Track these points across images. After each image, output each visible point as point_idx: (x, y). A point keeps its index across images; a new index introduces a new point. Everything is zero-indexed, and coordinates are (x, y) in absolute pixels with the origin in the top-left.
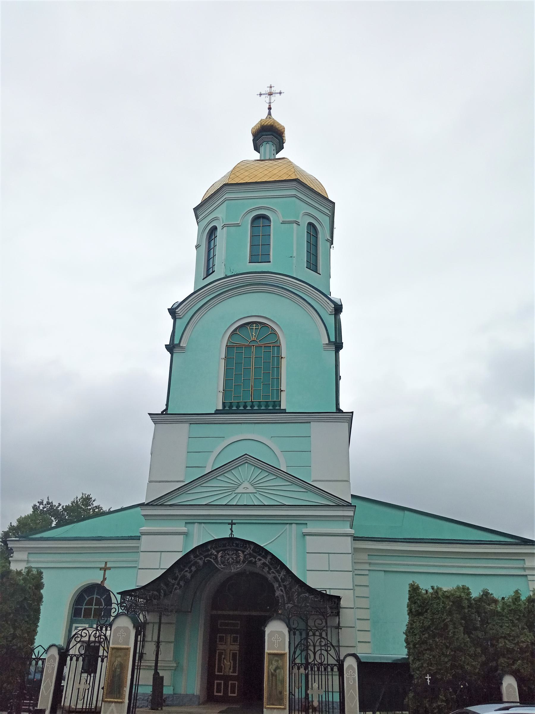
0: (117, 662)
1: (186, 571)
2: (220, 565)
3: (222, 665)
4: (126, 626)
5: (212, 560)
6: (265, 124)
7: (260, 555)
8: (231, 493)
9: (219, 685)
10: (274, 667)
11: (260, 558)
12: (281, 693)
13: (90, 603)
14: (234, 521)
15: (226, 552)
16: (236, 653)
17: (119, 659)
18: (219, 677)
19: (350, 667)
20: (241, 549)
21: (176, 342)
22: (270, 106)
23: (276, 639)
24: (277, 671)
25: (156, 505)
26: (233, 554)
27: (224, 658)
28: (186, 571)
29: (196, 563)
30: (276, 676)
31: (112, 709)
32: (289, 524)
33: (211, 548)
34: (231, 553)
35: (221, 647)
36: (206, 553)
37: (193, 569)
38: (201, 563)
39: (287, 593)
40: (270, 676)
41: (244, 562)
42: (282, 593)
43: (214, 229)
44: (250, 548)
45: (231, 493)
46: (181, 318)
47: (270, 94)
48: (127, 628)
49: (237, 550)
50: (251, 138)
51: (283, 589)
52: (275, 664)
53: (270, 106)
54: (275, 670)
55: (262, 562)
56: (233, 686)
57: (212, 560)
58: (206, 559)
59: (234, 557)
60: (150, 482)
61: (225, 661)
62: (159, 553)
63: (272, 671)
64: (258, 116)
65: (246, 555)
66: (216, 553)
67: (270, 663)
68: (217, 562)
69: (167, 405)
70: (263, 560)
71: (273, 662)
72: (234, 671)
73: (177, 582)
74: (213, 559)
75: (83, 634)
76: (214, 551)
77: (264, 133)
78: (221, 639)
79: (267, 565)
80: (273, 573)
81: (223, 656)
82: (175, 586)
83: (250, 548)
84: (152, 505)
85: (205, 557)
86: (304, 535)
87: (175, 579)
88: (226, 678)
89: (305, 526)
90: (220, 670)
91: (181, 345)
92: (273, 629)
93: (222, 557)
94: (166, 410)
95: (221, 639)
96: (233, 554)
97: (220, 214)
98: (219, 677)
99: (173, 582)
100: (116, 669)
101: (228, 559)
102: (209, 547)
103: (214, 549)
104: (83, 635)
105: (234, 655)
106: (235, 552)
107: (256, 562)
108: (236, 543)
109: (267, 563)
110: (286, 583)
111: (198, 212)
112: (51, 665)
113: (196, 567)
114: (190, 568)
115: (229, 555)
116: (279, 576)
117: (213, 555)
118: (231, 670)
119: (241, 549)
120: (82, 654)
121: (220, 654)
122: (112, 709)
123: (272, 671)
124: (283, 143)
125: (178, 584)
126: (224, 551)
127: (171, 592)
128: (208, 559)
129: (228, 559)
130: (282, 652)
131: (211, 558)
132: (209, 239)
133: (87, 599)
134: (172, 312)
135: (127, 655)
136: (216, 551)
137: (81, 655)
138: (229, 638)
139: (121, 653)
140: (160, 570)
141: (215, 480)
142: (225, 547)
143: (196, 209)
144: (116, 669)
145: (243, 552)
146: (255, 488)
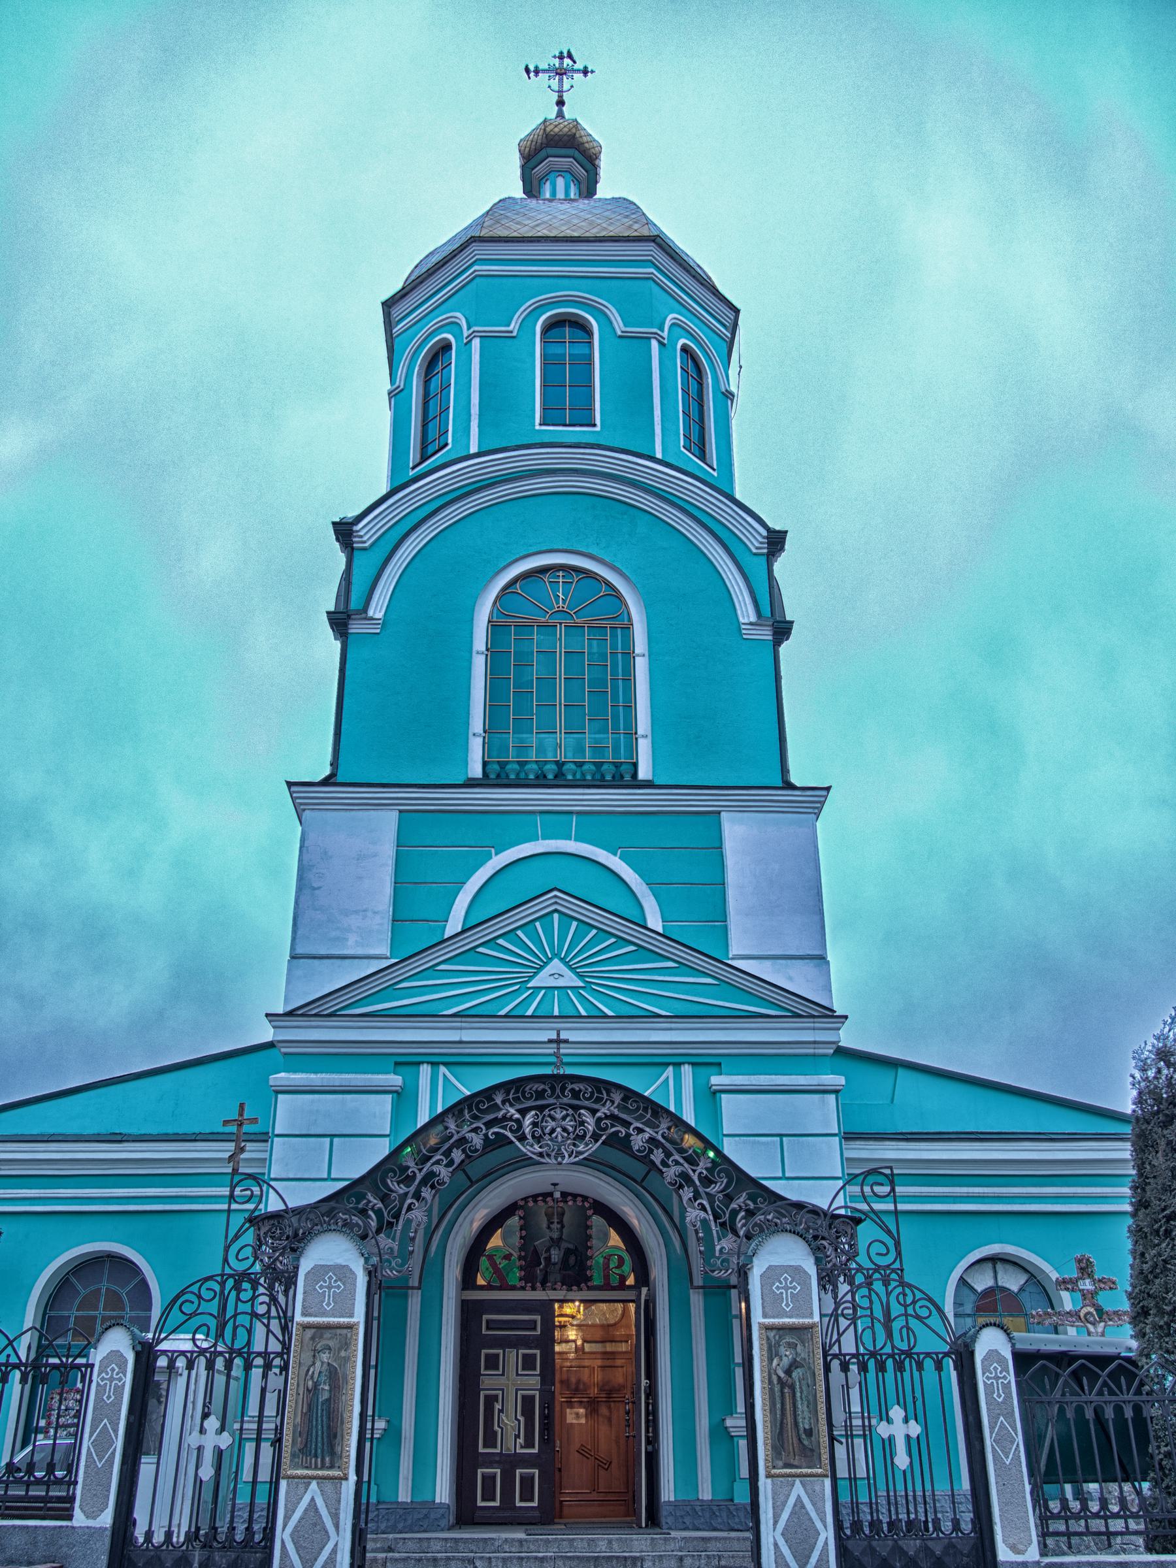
0: (318, 1364)
1: (438, 1162)
2: (532, 1146)
3: (496, 1428)
4: (341, 1261)
5: (509, 1134)
6: (556, 130)
7: (637, 1119)
8: (517, 987)
9: (489, 1480)
10: (786, 1362)
11: (641, 1126)
12: (809, 1433)
13: (90, 1302)
14: (563, 1036)
15: (546, 1112)
16: (533, 1397)
17: (325, 1357)
18: (489, 1461)
19: (993, 1355)
20: (587, 1103)
21: (354, 605)
22: (561, 97)
23: (786, 1288)
24: (794, 1374)
25: (316, 1015)
26: (564, 1118)
27: (501, 1411)
28: (438, 1162)
29: (463, 1140)
30: (792, 1387)
31: (313, 1499)
32: (674, 1064)
33: (504, 1102)
34: (559, 1115)
35: (489, 1381)
36: (492, 1116)
37: (457, 1156)
38: (477, 1141)
39: (716, 1217)
40: (777, 1388)
41: (595, 1137)
42: (703, 1214)
43: (446, 347)
44: (613, 1102)
45: (517, 987)
46: (365, 549)
47: (561, 73)
48: (346, 1267)
49: (576, 1108)
50: (516, 161)
51: (705, 1202)
52: (787, 1355)
53: (561, 97)
54: (788, 1372)
55: (647, 1136)
56: (527, 1481)
57: (509, 1134)
58: (492, 1131)
59: (569, 1124)
60: (294, 957)
61: (503, 1416)
62: (328, 1140)
63: (782, 1375)
64: (533, 110)
65: (599, 1120)
66: (517, 1116)
67: (772, 1352)
68: (523, 1138)
69: (334, 764)
70: (649, 1132)
71: (782, 1350)
72: (529, 1443)
73: (412, 1189)
74: (511, 1131)
75: (204, 1293)
76: (512, 1111)
77: (550, 151)
78: (492, 1362)
79: (658, 1144)
80: (677, 1163)
81: (498, 1406)
82: (409, 1201)
83: (613, 1102)
84: (302, 1015)
85: (489, 1125)
86: (715, 1093)
87: (408, 1180)
88: (510, 1462)
89: (715, 1069)
90: (490, 1440)
91: (371, 613)
92: (776, 1261)
93: (535, 1124)
94: (333, 775)
95: (492, 1362)
96: (564, 1118)
97: (455, 320)
98: (489, 1461)
99: (402, 1189)
100: (316, 1385)
101: (553, 1131)
102: (499, 1101)
103: (511, 1105)
104: (207, 1295)
105: (528, 1401)
106: (571, 1111)
107: (628, 1135)
108: (572, 1090)
109: (660, 1138)
110: (714, 1189)
111: (396, 312)
112: (111, 1379)
113: (464, 1151)
114: (447, 1153)
115: (553, 1119)
116: (694, 1171)
117: (511, 1119)
118: (521, 1441)
119: (587, 1103)
120: (205, 1350)
121: (490, 1400)
122: (313, 1499)
123: (782, 1375)
124: (596, 182)
125: (417, 1196)
126: (541, 1108)
127: (397, 1216)
128: (496, 1130)
129: (553, 1131)
130: (807, 1321)
131: (504, 1128)
132: (426, 375)
133: (83, 1292)
134: (344, 531)
135: (346, 1344)
136: (518, 1111)
137: (202, 1352)
138: (513, 1357)
139: (328, 1340)
140: (329, 1183)
141: (472, 952)
142: (544, 1098)
143: (388, 305)
144: (316, 1385)
145: (594, 1112)
146: (580, 976)
